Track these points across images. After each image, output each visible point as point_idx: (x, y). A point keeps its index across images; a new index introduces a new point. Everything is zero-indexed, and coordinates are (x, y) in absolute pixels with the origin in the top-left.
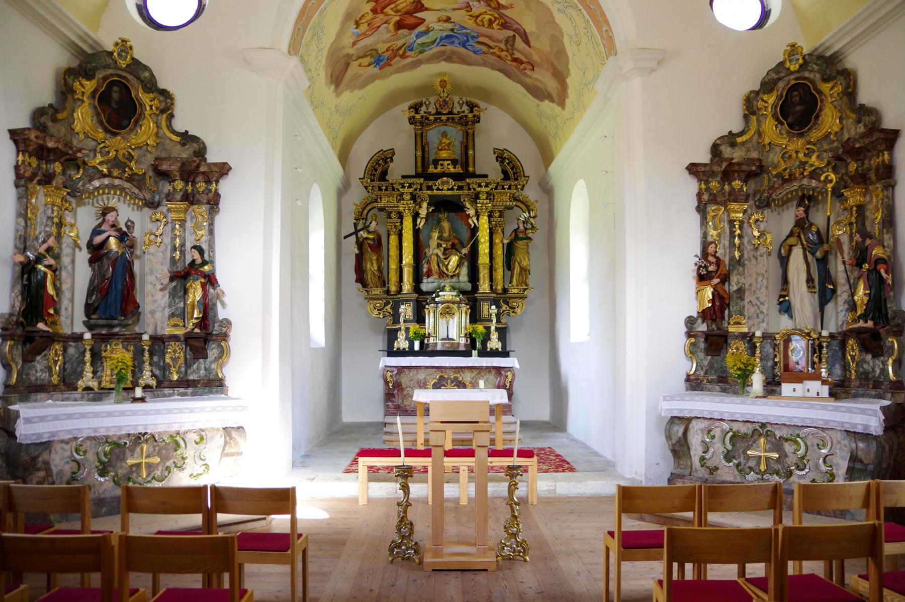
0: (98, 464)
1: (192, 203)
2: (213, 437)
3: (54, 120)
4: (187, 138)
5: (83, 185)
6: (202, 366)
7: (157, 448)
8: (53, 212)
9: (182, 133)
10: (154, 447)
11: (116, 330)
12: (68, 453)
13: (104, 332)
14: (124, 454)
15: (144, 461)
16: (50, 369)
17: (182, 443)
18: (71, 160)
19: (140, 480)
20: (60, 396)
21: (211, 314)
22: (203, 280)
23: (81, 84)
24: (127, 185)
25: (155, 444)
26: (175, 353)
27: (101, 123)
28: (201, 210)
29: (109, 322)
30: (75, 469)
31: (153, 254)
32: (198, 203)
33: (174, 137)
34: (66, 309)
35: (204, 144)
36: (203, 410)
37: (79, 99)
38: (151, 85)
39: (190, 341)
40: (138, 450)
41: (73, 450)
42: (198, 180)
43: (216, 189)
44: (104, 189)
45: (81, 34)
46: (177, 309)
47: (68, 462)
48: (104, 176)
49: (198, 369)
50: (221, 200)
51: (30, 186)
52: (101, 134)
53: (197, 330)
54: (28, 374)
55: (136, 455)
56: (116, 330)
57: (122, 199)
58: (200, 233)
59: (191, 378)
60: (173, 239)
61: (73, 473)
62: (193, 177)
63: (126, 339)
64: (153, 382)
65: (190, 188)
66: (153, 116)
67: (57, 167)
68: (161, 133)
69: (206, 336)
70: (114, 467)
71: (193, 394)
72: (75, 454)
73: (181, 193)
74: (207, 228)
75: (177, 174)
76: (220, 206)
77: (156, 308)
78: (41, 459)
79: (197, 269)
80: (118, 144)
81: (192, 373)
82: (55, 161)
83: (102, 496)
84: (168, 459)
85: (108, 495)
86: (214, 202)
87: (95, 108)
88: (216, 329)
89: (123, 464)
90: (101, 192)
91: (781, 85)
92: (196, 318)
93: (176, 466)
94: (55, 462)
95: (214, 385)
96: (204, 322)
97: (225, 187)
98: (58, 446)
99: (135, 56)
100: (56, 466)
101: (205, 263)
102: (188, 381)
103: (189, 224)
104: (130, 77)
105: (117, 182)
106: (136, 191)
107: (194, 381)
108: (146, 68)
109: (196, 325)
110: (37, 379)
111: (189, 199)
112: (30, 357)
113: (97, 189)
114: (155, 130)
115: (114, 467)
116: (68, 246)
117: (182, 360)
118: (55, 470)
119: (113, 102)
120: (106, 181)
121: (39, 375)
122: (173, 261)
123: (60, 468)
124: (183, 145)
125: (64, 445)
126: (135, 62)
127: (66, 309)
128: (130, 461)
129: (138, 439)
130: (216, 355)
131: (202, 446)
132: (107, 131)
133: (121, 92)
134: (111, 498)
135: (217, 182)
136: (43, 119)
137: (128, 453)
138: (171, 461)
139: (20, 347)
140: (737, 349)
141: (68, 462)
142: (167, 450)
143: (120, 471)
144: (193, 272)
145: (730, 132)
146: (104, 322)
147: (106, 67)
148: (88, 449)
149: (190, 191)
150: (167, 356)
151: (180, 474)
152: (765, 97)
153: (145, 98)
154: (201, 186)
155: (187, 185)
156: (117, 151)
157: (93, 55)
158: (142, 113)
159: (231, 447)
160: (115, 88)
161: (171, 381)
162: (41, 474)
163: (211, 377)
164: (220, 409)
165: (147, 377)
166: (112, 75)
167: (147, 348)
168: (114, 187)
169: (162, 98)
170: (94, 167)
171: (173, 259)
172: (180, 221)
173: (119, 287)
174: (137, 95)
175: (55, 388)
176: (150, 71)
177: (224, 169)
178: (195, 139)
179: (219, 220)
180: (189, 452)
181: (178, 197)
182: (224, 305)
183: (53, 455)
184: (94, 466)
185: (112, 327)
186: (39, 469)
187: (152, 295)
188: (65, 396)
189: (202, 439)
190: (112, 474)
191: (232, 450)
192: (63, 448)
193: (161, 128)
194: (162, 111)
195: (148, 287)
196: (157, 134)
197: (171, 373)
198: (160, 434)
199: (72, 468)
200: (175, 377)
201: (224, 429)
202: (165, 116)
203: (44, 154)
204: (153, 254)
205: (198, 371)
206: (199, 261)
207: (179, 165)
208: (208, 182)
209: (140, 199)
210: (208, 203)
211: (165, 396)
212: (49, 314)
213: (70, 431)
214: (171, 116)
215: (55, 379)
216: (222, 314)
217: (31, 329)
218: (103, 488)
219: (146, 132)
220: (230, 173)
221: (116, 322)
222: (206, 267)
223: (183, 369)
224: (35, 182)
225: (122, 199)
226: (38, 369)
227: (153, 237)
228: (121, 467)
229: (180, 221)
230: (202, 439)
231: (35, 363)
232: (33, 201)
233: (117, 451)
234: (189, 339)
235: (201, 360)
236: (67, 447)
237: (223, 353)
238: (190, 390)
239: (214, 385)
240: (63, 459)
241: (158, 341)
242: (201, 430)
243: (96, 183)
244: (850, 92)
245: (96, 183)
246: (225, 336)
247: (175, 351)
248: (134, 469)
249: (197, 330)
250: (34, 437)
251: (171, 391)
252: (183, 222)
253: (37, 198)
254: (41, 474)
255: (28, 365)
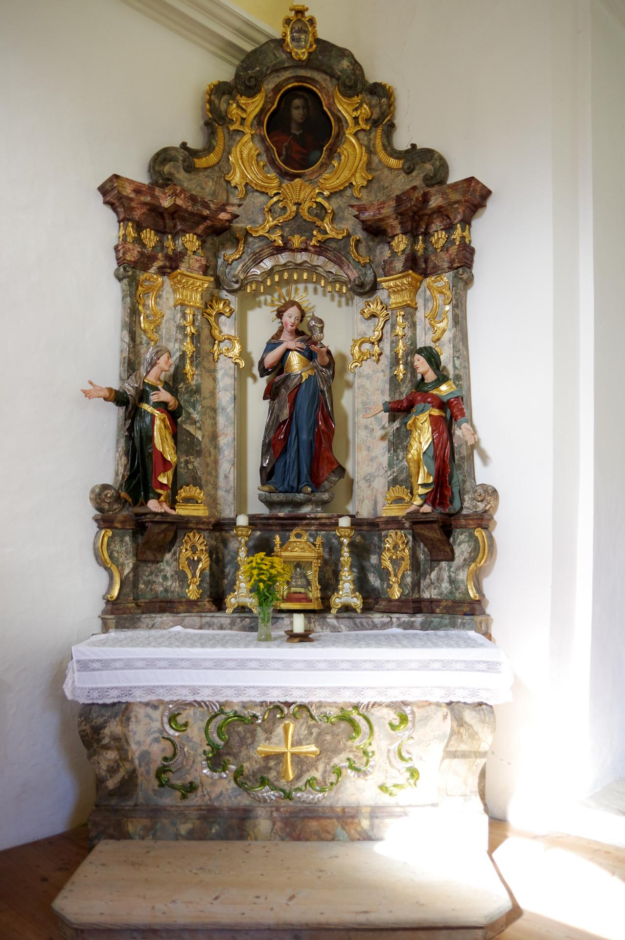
0: (208, 748)
1: (425, 274)
2: (426, 719)
3: (190, 169)
4: (416, 157)
5: (246, 270)
6: (445, 575)
7: (315, 731)
8: (184, 316)
9: (407, 151)
10: (309, 728)
11: (306, 510)
12: (157, 725)
13: (281, 514)
14: (254, 735)
15: (290, 750)
16: (181, 577)
17: (362, 723)
18: (219, 233)
19: (282, 783)
20: (197, 619)
21: (458, 476)
22: (436, 412)
23: (239, 106)
24: (319, 260)
25: (312, 722)
26: (395, 549)
27: (272, 162)
28: (441, 284)
29: (290, 496)
30: (169, 754)
31: (368, 377)
32: (436, 271)
33: (393, 162)
34: (226, 477)
35: (441, 159)
36: (401, 665)
37: (237, 131)
38: (355, 83)
39: (419, 529)
40: (280, 730)
41: (166, 720)
42: (434, 227)
43: (463, 238)
44: (280, 273)
45: (238, 24)
46: (401, 471)
47: (156, 740)
48: (279, 250)
49: (439, 579)
50: (476, 258)
51: (142, 276)
52: (273, 181)
53: (427, 508)
54: (148, 583)
55: (274, 740)
56: (306, 510)
57: (320, 290)
58: (441, 325)
59: (426, 595)
60: (395, 344)
61: (165, 759)
62: (427, 222)
63: (323, 525)
64: (356, 602)
65: (420, 247)
66: (361, 135)
67: (190, 241)
68: (375, 160)
69: (448, 514)
70: (235, 756)
71: (424, 627)
72: (167, 727)
73: (403, 258)
74: (450, 315)
75: (395, 223)
76: (475, 270)
77: (373, 470)
78: (107, 731)
79: (426, 392)
80: (302, 193)
81: (428, 587)
82: (184, 232)
83: (216, 804)
84: (336, 751)
85: (225, 803)
86: (464, 260)
87: (263, 140)
88: (469, 505)
89: (252, 753)
90: (277, 278)
91: (269, 85)
92: (424, 485)
93: (351, 767)
94: (137, 738)
95: (463, 611)
96: (443, 488)
97: (483, 232)
98: (141, 712)
99: (321, 35)
100: (138, 743)
101: (442, 378)
102: (419, 601)
103: (420, 314)
104: (318, 76)
105: (301, 257)
106: (334, 269)
107: (431, 601)
108: (343, 53)
109: (426, 499)
110: (166, 590)
111: (419, 266)
112: (150, 555)
113: (270, 272)
114: (365, 158)
115: (235, 756)
116: (226, 374)
117: (406, 564)
118: (135, 750)
119: (294, 126)
120: (283, 258)
121: (169, 583)
122: (394, 382)
123: (144, 748)
124: (409, 172)
125: (149, 710)
126: (324, 46)
127: (226, 477)
128: (264, 748)
129: (278, 709)
130: (466, 555)
131: (403, 732)
132: (283, 175)
133: (306, 107)
134: (230, 809)
135: (466, 222)
136: (167, 169)
137: (261, 734)
138: (344, 755)
139: (127, 539)
140: (194, 549)
141: (156, 740)
142: (334, 735)
143: (246, 765)
144: (431, 398)
145: (184, 145)
146: (281, 497)
147: (277, 69)
148: (191, 721)
149: (420, 252)
150: (386, 555)
151: (361, 782)
152: (243, 100)
153: (344, 108)
154: (439, 238)
155: (415, 242)
156: (298, 204)
157: (254, 52)
158: (340, 135)
159: (461, 740)
160: (297, 102)
161: (390, 600)
162: (112, 755)
163: (458, 596)
164: (436, 665)
165: (346, 593)
166: (288, 80)
167: (346, 541)
168: (299, 267)
169: (374, 101)
170: (262, 238)
171: (393, 379)
172: (402, 308)
173: (304, 436)
174: (331, 105)
175: (191, 606)
176: (350, 56)
177: (475, 197)
178: (428, 154)
179: (475, 297)
180: (381, 743)
181: (399, 265)
182: (485, 458)
183: (133, 726)
184: (201, 751)
185: (300, 504)
186: (107, 747)
187: (368, 449)
188: (204, 620)
189: (404, 719)
190: (233, 767)
191: (463, 747)
192: (148, 716)
193: (375, 153)
194: (375, 123)
195: (362, 434)
196: (369, 163)
197: (390, 586)
198: (320, 705)
199: (163, 750)
200: (396, 594)
201: (450, 704)
202: (379, 130)
203: (164, 219)
204: (368, 377)
205: (438, 584)
206: (431, 376)
207: (393, 203)
208: (449, 228)
209: (343, 283)
210: (451, 268)
211: (374, 627)
212: (161, 484)
213: (151, 690)
214: (392, 126)
215: (192, 592)
216: (482, 475)
217: (139, 510)
218: (217, 790)
219: (350, 162)
220: (490, 203)
221: (300, 496)
222: (444, 388)
223: (409, 580)
224: (153, 270)
225: (320, 290)
226: (169, 575)
227: (366, 346)
228: (249, 758)
229: (402, 308)
230: (404, 719)
231: (163, 566)
232: (151, 302)
233: (240, 729)
234: (416, 521)
235: (444, 564)
236: (156, 714)
237: (483, 552)
238: (419, 619)
239: (463, 611)
240: (148, 733)
241: (369, 530)
242: (405, 704)
243: (267, 264)
244: (383, 121)
245: (267, 264)
246: (484, 520)
247: (194, 549)
248: (272, 763)
249: (427, 508)
250: (115, 693)
251: (386, 619)
252: (410, 310)
253: (158, 296)
254: (112, 755)
255: (147, 569)
